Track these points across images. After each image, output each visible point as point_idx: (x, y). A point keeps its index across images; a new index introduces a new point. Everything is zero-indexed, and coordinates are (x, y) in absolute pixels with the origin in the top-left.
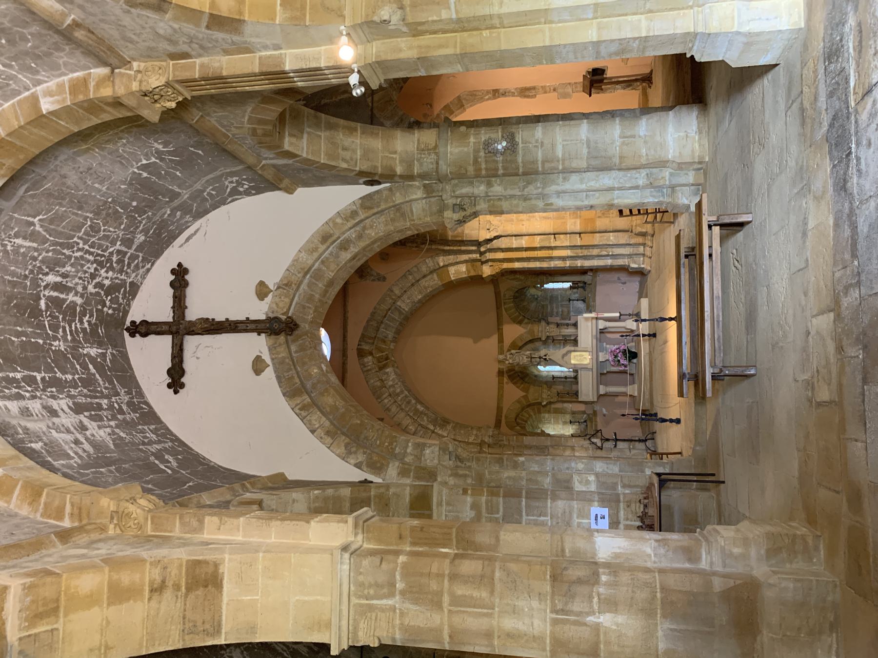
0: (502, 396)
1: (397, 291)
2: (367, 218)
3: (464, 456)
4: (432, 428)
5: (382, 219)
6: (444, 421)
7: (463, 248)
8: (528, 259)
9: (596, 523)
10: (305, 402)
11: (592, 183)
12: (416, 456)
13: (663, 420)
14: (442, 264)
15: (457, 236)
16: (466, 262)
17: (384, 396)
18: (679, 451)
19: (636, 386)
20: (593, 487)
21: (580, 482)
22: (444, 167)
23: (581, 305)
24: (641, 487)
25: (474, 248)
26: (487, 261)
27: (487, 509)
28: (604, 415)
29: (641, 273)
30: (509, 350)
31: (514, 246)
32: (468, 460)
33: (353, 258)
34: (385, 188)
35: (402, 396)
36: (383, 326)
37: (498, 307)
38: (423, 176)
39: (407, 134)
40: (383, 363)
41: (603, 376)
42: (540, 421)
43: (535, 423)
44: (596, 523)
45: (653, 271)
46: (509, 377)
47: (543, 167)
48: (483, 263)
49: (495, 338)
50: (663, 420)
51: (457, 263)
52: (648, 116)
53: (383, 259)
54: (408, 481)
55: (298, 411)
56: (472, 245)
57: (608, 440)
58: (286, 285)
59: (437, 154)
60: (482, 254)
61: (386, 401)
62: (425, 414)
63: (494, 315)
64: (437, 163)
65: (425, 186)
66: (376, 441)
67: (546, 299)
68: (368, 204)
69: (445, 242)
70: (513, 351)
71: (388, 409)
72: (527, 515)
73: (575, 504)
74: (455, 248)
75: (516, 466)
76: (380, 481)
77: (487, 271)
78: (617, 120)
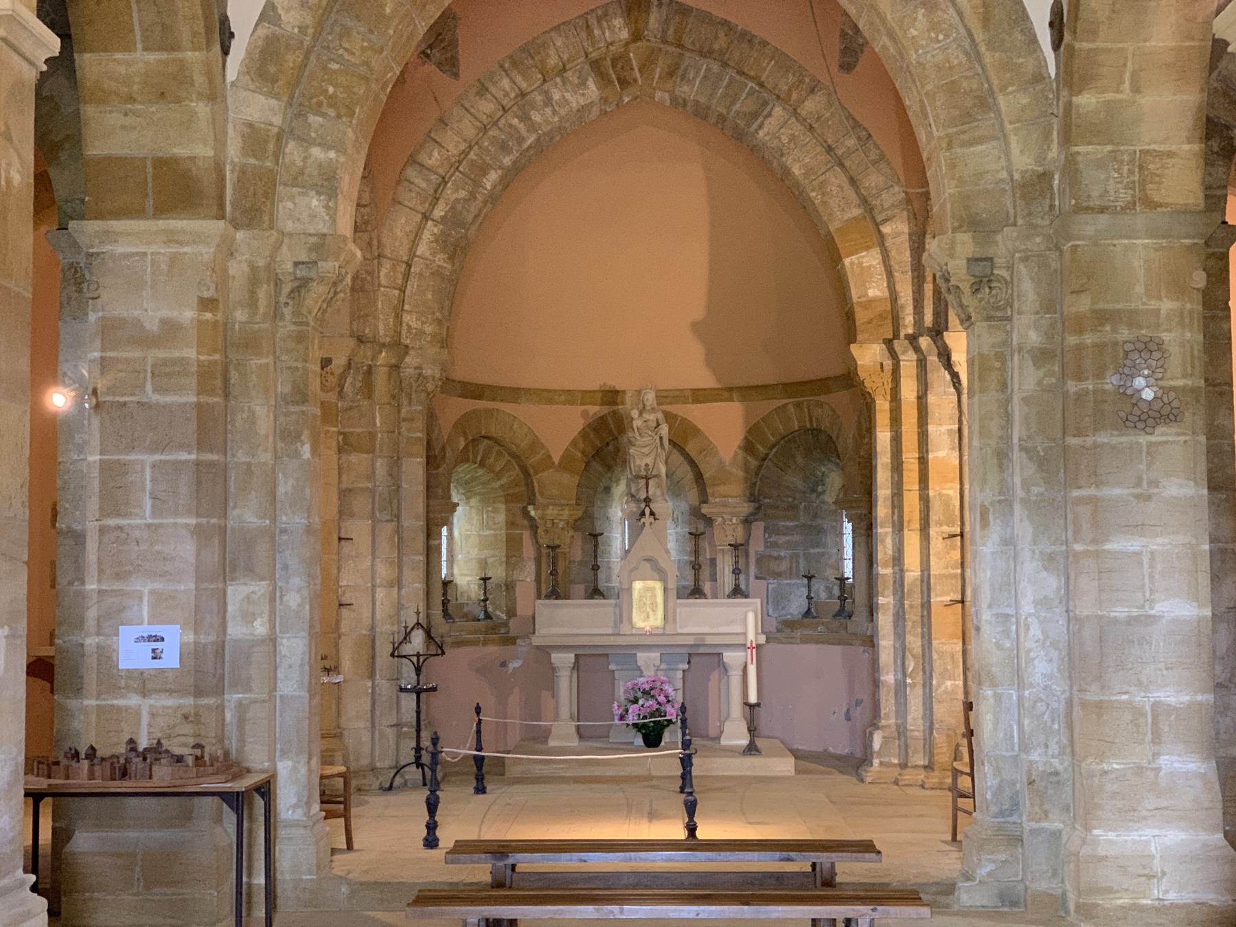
0: (551, 401)
1: (812, 105)
2: (960, 14)
3: (309, 302)
4: (438, 213)
5: (957, 58)
6: (455, 245)
8: (897, 466)
9: (141, 639)
11: (1035, 631)
12: (301, 172)
13: (432, 806)
14: (886, 229)
17: (519, 79)
18: (355, 847)
19: (575, 743)
20: (235, 630)
21: (248, 598)
22: (1089, 230)
23: (796, 605)
24: (240, 750)
25: (929, 319)
26: (893, 355)
27: (166, 362)
28: (504, 664)
29: (856, 763)
30: (669, 417)
31: (931, 428)
32: (297, 313)
34: (1042, 63)
36: (715, 67)
37: (791, 388)
38: (1071, 168)
39: (1189, 122)
40: (612, 71)
41: (592, 661)
42: (486, 501)
43: (479, 489)
44: (141, 639)
45: (859, 788)
46: (603, 419)
47: (1080, 501)
48: (889, 343)
49: (708, 381)
50: (432, 806)
52: (1213, 777)
54: (234, 149)
56: (936, 314)
57: (418, 670)
59: (1131, 206)
60: (913, 339)
61: (506, 83)
62: (472, 195)
63: (768, 376)
64: (1102, 210)
65: (1045, 177)
66: (339, 60)
67: (815, 516)
70: (664, 430)
71: (482, 91)
72: (154, 466)
73: (187, 586)
75: (288, 436)
76: (231, 75)
77: (868, 355)
78: (1210, 698)
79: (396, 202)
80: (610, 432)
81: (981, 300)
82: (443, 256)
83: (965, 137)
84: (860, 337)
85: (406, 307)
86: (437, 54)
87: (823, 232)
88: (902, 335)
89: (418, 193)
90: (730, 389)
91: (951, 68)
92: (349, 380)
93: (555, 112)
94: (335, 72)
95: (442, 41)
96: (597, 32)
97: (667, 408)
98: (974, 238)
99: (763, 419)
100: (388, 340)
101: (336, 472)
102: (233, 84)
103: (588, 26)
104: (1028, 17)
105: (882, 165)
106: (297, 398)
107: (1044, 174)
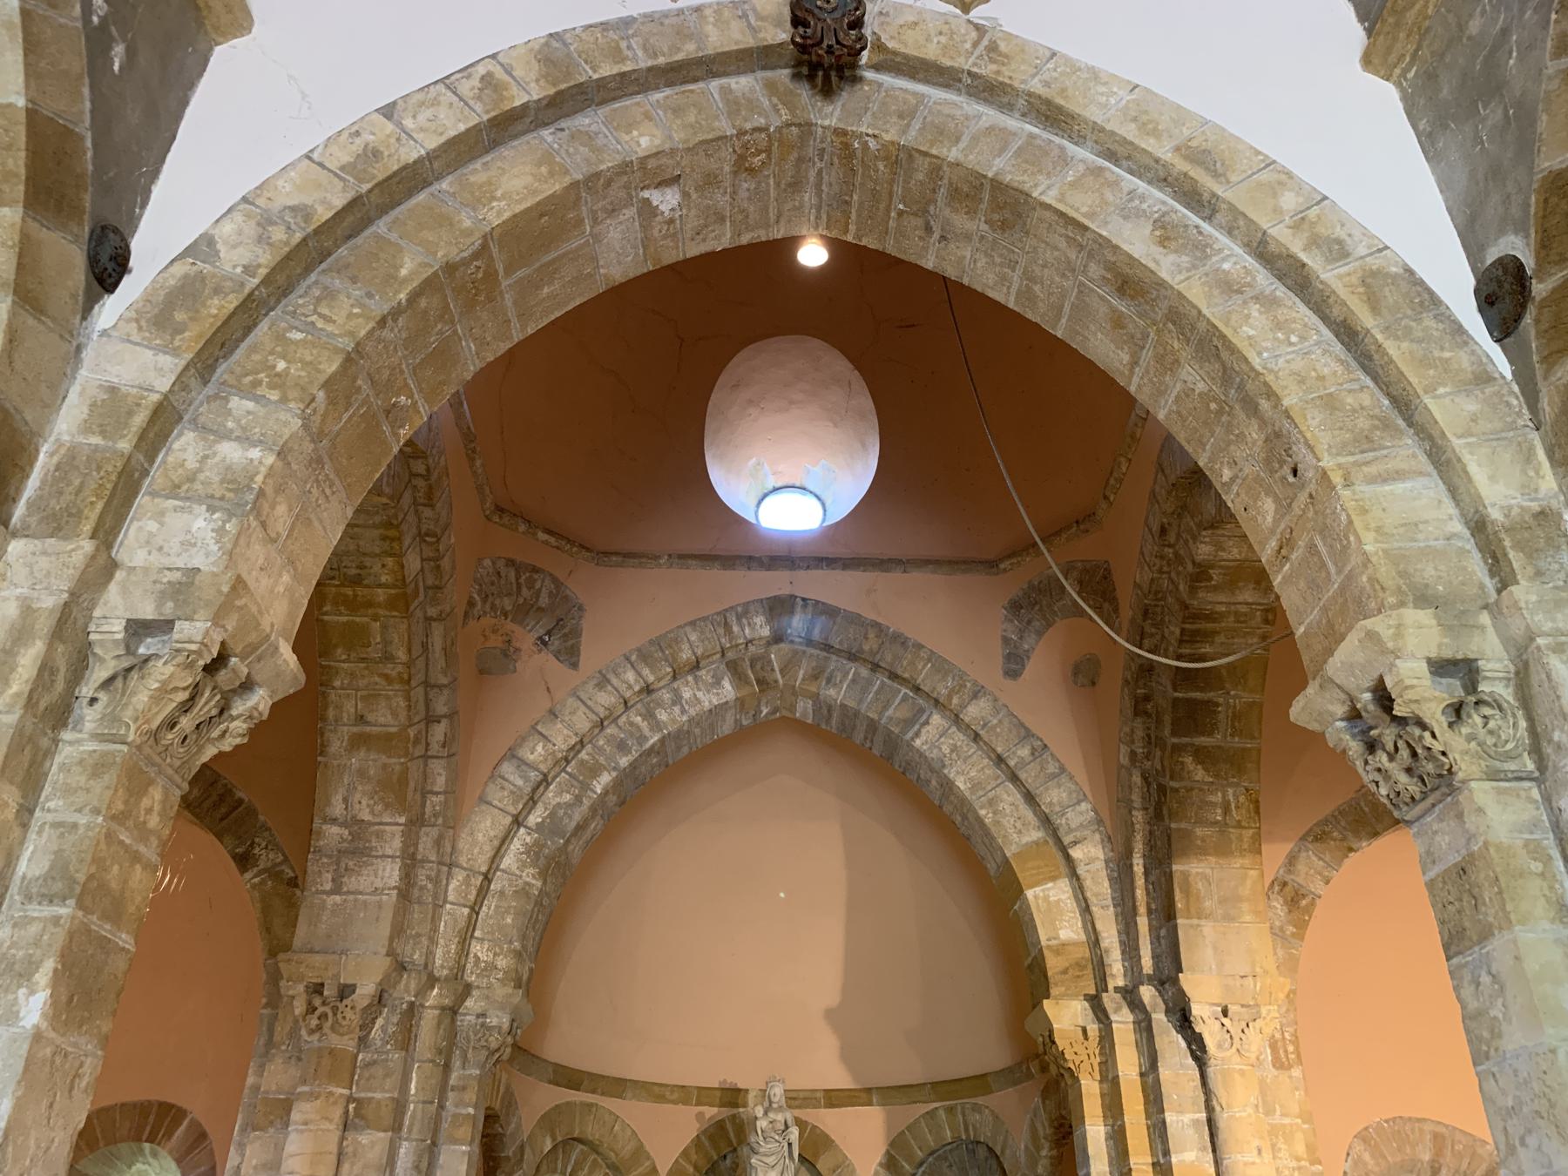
1: (975, 711)
4: (534, 819)
7: (1143, 922)
10: (515, 90)
12: (191, 478)
14: (1076, 853)
15: (1187, 892)
16: (1094, 941)
17: (646, 672)
30: (800, 1123)
31: (1170, 1117)
33: (1131, 282)
35: (644, 725)
36: (864, 672)
46: (720, 1125)
48: (1095, 1003)
49: (841, 1079)
51: (1086, 910)
53: (1076, 671)
55: (481, 70)
56: (1156, 957)
58: (993, 48)
61: (630, 676)
62: (578, 799)
63: (913, 1072)
68: (1390, 296)
69: (1163, 855)
70: (794, 1133)
71: (603, 682)
74: (1140, 894)
77: (1066, 1015)
79: (483, 800)
80: (731, 1144)
81: (1471, 738)
82: (532, 871)
83: (1372, 470)
84: (1054, 991)
85: (477, 934)
86: (556, 643)
87: (992, 867)
88: (1111, 987)
89: (512, 792)
90: (869, 1090)
91: (1321, 378)
92: (380, 1022)
93: (683, 711)
94: (296, 343)
95: (563, 627)
96: (736, 629)
97: (797, 1112)
98: (1437, 617)
99: (908, 1128)
100: (445, 972)
101: (334, 1158)
102: (104, 333)
103: (726, 623)
104: (1441, 302)
105: (1064, 779)
106: (58, 886)
107: (1542, 513)
